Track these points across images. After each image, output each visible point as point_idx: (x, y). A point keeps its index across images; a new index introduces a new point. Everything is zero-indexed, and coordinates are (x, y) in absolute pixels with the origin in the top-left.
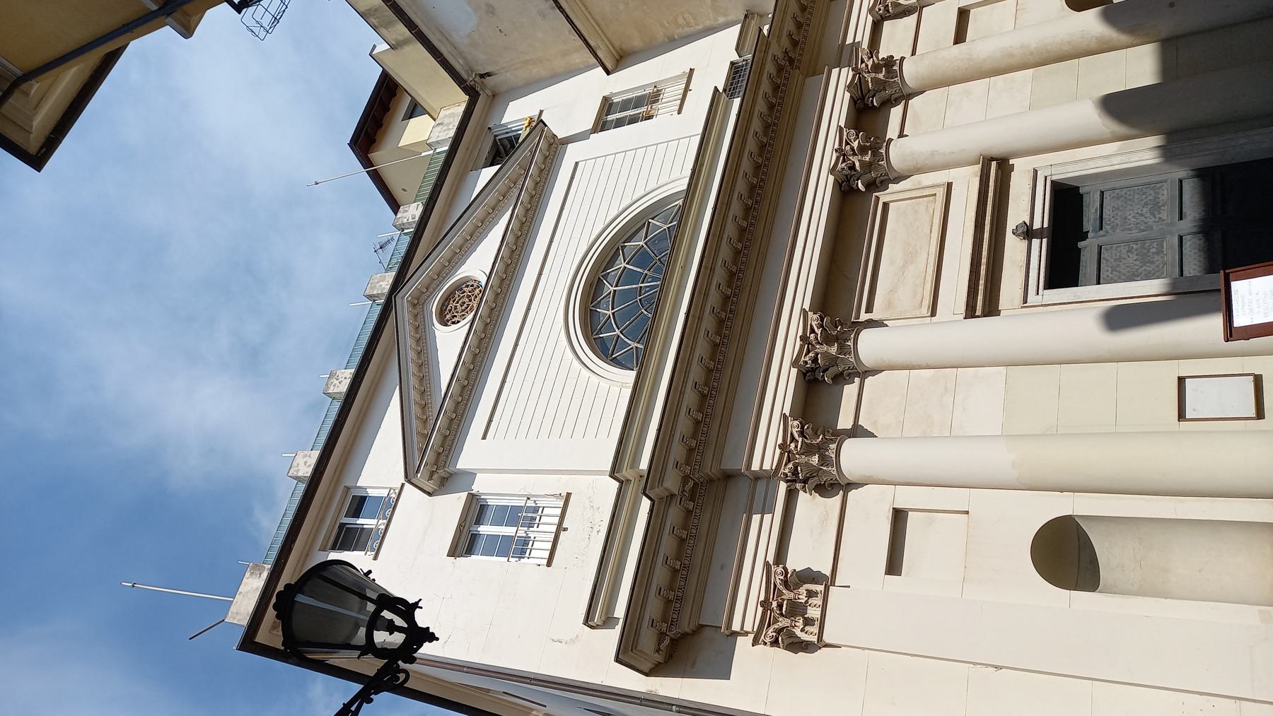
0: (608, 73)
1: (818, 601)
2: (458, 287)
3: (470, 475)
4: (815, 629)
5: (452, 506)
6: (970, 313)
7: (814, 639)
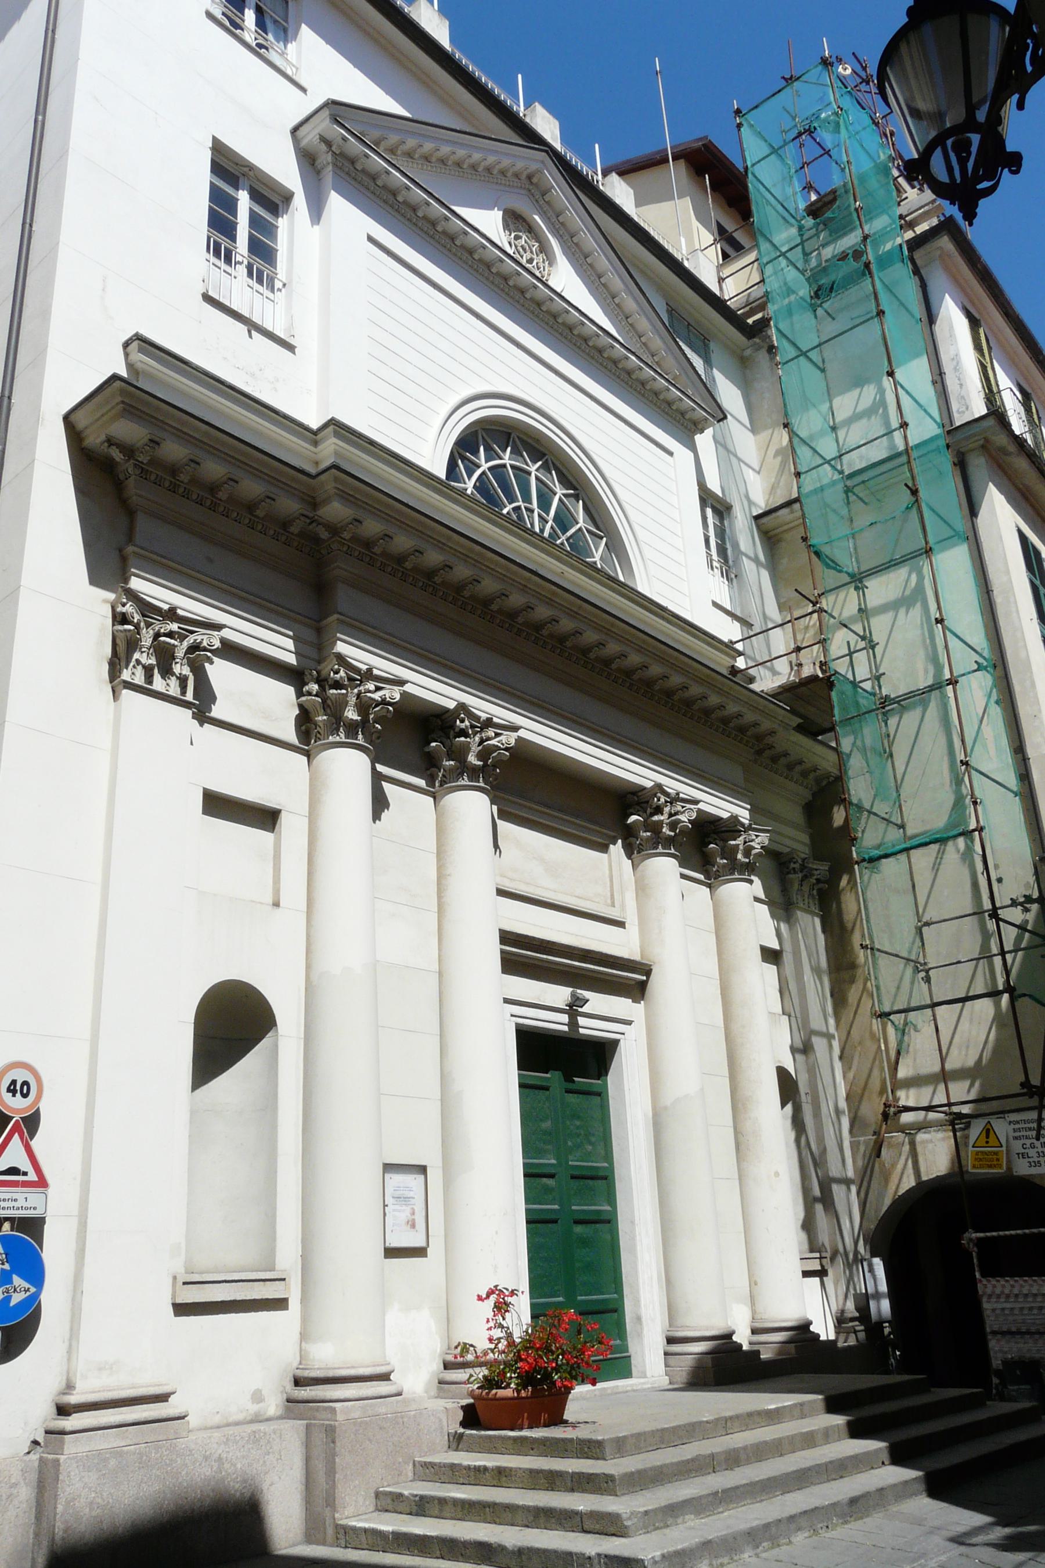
0: (757, 518)
1: (174, 690)
2: (544, 249)
3: (317, 209)
4: (139, 679)
5: (283, 167)
6: (507, 937)
7: (126, 675)
